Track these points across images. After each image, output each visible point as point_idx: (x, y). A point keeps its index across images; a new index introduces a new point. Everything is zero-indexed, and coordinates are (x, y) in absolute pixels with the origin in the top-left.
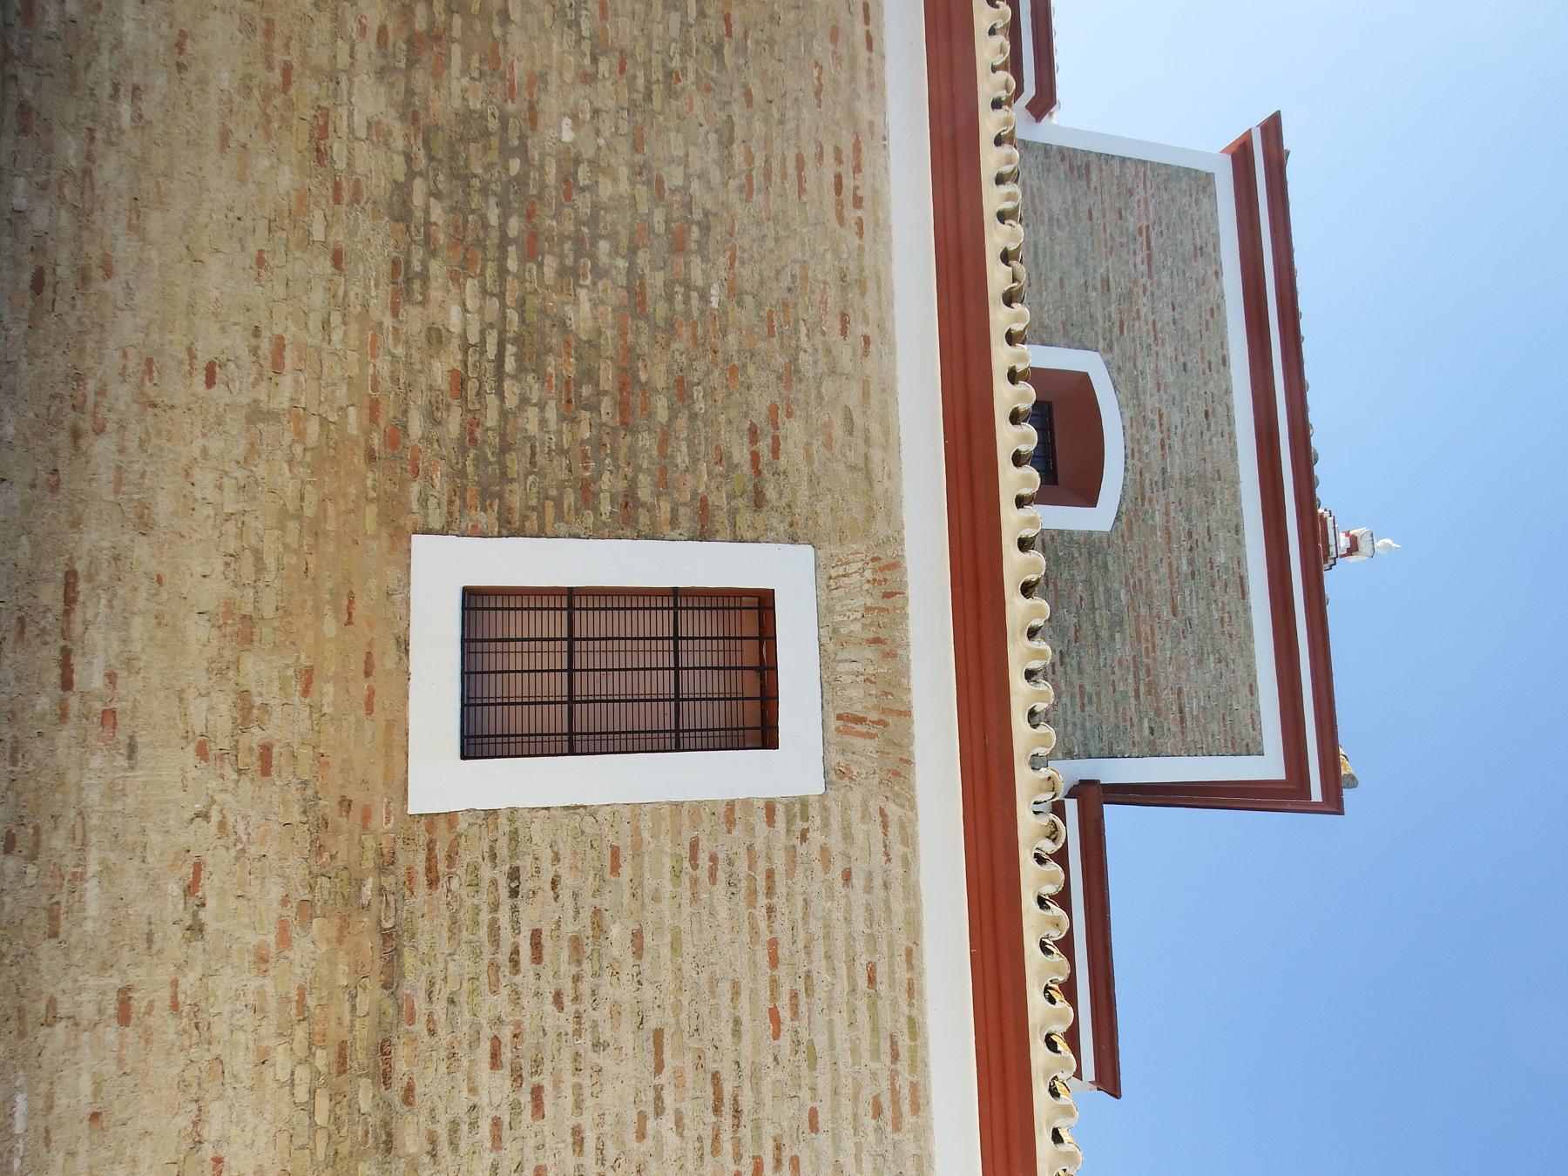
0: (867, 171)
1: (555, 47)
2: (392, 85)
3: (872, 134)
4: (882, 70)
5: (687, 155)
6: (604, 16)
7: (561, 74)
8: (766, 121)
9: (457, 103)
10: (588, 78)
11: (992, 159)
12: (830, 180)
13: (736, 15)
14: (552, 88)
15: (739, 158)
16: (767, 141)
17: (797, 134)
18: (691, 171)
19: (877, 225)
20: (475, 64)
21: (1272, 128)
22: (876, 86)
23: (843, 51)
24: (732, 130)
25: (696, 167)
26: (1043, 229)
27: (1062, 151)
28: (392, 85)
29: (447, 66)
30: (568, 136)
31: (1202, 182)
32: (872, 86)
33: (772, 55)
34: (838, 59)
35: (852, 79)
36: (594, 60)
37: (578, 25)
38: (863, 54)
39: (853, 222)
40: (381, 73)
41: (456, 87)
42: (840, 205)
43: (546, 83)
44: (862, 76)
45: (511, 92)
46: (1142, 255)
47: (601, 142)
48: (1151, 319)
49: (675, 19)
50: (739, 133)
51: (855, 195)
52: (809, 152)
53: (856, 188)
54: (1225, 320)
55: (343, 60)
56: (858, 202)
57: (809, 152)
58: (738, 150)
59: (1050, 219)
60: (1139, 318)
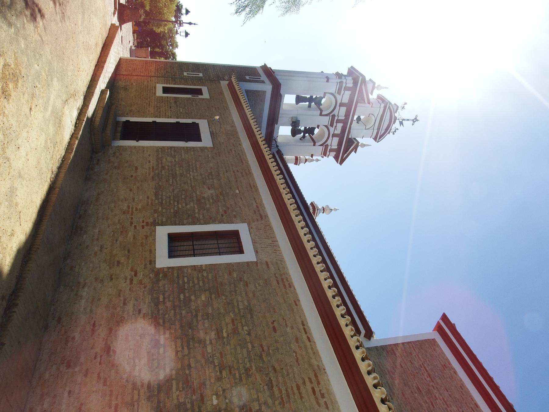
0: (322, 383)
1: (207, 371)
2: (152, 401)
3: (320, 369)
4: (316, 347)
5: (258, 396)
6: (222, 357)
7: (210, 380)
8: (283, 376)
9: (175, 402)
10: (219, 379)
11: (358, 354)
12: (310, 390)
13: (264, 344)
14: (208, 386)
15: (277, 392)
16: (285, 383)
17: (294, 377)
18: (261, 402)
19: (332, 403)
20: (181, 385)
21: (444, 318)
22: (316, 353)
23: (302, 345)
24: (272, 383)
25: (262, 400)
26: (387, 376)
27: (382, 347)
28: (152, 401)
29: (172, 389)
30: (215, 402)
31: (433, 342)
32: (314, 353)
33: (279, 353)
34: (300, 347)
35: (307, 353)
36: (221, 372)
37: (214, 362)
38: (308, 344)
39: (323, 404)
40: (149, 398)
41: (175, 396)
42: (317, 399)
43: (206, 385)
44: (310, 351)
45: (194, 392)
46: (426, 374)
47: (227, 401)
48: (441, 397)
49: (245, 351)
50: (274, 383)
51: (321, 393)
52: (300, 382)
53: (320, 390)
54: (467, 388)
55: (136, 397)
56: (323, 396)
57: (300, 382)
58: (275, 389)
59: (388, 371)
60: (437, 399)
